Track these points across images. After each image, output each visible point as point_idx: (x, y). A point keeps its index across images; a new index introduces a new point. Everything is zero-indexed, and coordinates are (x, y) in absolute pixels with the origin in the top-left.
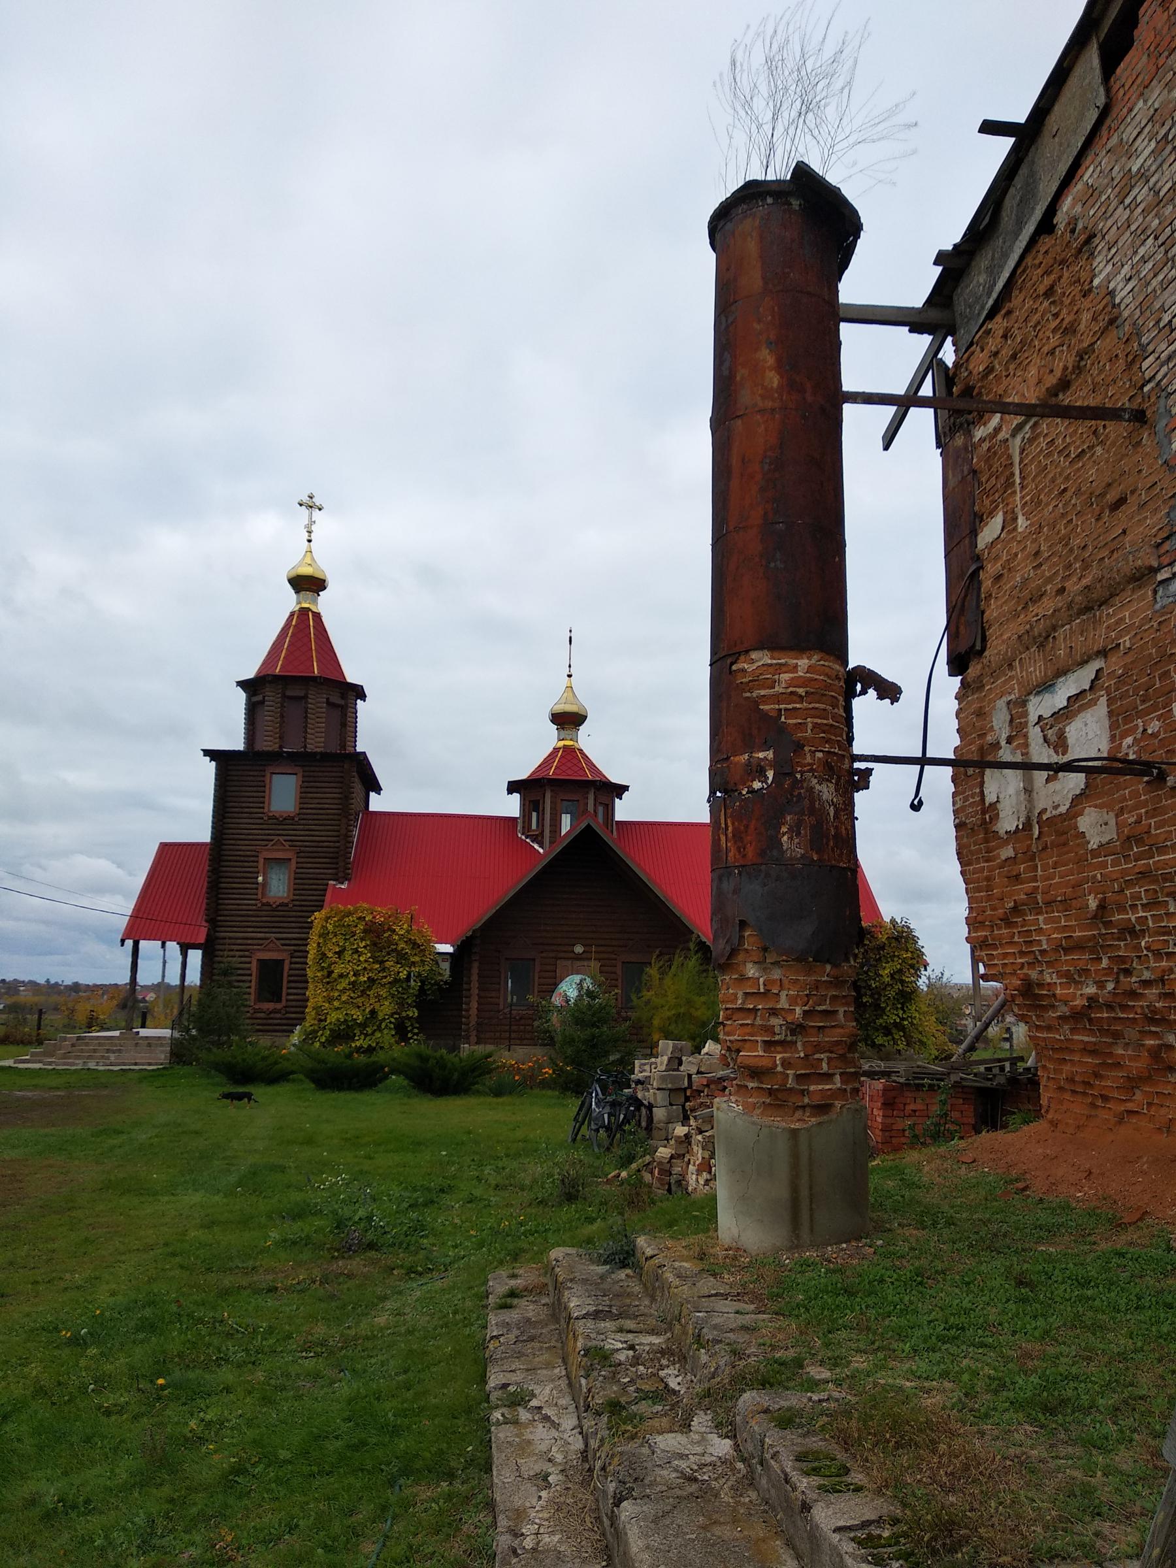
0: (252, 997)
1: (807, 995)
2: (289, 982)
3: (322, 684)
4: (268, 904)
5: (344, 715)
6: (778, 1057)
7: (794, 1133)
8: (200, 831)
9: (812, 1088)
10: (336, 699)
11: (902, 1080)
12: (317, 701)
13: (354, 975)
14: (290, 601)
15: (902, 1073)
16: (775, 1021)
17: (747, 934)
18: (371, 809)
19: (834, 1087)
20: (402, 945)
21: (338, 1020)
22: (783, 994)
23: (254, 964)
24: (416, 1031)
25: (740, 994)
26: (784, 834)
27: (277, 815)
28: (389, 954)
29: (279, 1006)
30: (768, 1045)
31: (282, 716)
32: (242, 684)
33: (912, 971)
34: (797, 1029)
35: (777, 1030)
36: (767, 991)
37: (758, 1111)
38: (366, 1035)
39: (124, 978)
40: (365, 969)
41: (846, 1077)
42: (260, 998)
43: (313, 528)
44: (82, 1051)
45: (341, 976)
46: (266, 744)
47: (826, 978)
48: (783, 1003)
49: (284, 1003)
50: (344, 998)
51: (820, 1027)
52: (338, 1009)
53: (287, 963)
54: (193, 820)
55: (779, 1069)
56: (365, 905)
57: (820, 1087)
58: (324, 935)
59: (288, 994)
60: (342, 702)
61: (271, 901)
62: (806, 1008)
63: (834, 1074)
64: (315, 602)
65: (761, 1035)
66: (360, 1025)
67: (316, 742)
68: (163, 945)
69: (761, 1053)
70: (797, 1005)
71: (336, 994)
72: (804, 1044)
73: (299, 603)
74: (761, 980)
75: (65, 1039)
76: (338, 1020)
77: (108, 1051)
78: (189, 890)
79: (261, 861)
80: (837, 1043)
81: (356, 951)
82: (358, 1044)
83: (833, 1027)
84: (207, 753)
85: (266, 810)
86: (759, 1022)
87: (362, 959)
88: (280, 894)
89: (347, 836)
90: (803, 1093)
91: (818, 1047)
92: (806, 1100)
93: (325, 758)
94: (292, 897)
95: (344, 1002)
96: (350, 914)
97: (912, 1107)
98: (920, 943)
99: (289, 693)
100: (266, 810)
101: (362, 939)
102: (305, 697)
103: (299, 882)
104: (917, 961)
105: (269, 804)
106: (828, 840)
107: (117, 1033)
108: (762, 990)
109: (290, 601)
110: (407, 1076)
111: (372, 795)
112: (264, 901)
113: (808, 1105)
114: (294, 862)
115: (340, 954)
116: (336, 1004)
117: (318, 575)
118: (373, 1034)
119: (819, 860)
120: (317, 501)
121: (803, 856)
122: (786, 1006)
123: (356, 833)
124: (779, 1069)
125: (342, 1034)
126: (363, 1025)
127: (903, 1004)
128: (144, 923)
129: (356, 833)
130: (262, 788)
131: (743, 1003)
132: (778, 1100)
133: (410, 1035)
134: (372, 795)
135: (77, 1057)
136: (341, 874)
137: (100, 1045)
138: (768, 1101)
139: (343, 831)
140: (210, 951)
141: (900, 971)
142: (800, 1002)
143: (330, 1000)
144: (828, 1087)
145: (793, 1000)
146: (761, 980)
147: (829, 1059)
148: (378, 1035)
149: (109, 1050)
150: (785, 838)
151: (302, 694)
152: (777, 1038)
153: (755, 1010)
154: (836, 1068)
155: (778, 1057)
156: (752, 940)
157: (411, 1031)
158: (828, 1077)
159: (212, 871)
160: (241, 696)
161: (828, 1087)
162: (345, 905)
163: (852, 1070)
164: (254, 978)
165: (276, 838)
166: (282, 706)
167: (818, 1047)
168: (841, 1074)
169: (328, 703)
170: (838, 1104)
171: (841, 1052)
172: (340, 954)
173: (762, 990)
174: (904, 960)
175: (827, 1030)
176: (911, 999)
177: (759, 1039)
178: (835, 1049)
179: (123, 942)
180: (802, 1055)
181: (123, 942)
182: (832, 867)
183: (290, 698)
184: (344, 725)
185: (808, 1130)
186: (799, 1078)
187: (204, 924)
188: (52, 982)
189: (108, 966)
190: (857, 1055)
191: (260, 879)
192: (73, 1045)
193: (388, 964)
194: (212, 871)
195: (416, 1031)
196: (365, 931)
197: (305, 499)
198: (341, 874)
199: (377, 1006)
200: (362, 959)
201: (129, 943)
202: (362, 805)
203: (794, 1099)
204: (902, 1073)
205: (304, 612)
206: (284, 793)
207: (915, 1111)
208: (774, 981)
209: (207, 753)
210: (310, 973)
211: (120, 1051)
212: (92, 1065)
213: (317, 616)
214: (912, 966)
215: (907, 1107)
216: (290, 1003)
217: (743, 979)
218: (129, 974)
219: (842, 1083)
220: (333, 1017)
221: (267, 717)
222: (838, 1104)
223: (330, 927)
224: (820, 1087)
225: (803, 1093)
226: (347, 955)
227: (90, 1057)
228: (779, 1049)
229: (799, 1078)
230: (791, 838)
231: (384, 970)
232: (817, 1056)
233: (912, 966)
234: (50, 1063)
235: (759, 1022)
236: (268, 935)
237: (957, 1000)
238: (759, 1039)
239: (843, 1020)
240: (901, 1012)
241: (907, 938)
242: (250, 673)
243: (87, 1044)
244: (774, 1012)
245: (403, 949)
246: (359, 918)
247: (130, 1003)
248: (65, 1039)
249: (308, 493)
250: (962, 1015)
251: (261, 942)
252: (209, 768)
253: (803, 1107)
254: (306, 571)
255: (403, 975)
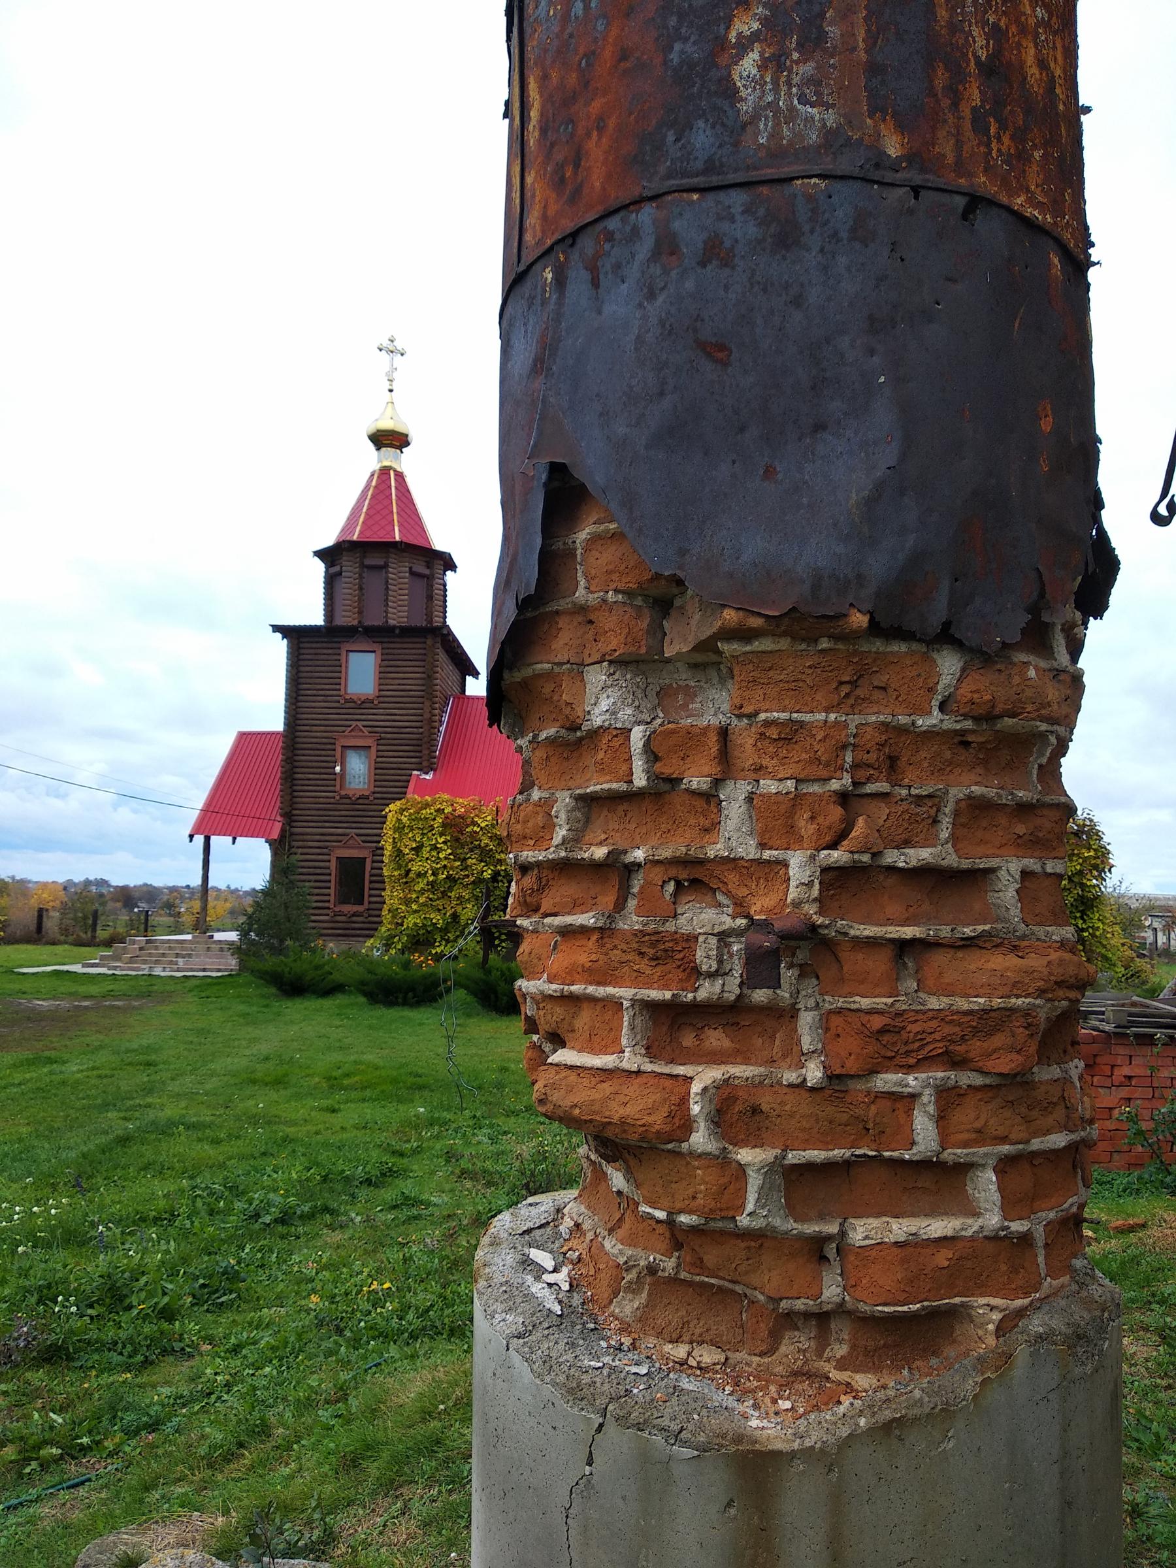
0: (332, 898)
1: (843, 798)
2: (371, 882)
3: (403, 551)
4: (347, 797)
5: (430, 587)
6: (704, 1077)
7: (755, 1471)
8: (274, 720)
9: (862, 1231)
10: (420, 568)
11: (1108, 1028)
12: (399, 571)
13: (433, 874)
14: (371, 460)
15: (1109, 1015)
16: (702, 918)
17: (582, 536)
18: (468, 693)
19: (972, 1226)
20: (486, 841)
21: (415, 924)
22: (735, 796)
23: (334, 861)
24: (504, 937)
25: (564, 801)
26: (744, 45)
27: (355, 698)
28: (471, 850)
29: (360, 908)
30: (670, 1024)
31: (361, 589)
32: (321, 554)
33: (1095, 873)
34: (793, 948)
35: (705, 956)
36: (664, 786)
37: (627, 1306)
38: (448, 941)
39: (196, 881)
40: (445, 867)
41: (1025, 1176)
42: (343, 899)
43: (395, 375)
44: (150, 955)
45: (419, 875)
46: (345, 619)
47: (933, 719)
48: (734, 834)
49: (366, 905)
50: (422, 900)
51: (903, 947)
52: (416, 912)
53: (368, 862)
54: (261, 700)
55: (701, 1139)
56: (445, 796)
57: (900, 1228)
58: (399, 828)
59: (370, 896)
60: (427, 572)
61: (350, 794)
62: (836, 856)
63: (964, 1169)
64: (397, 459)
65: (638, 980)
66: (441, 930)
67: (398, 617)
68: (234, 839)
69: (630, 1060)
70: (792, 839)
71: (414, 896)
72: (826, 1020)
73: (380, 461)
74: (637, 736)
75: (134, 942)
76: (415, 924)
77: (177, 955)
78: (276, 783)
79: (339, 749)
80: (987, 1022)
81: (434, 848)
82: (439, 950)
83: (969, 944)
84: (276, 628)
85: (342, 692)
86: (632, 921)
87: (441, 856)
88: (361, 786)
89: (431, 721)
90: (817, 1250)
91: (893, 1042)
92: (831, 1291)
93: (407, 632)
94: (372, 789)
95: (423, 905)
96: (427, 805)
97: (1126, 1071)
98: (1106, 839)
99: (367, 562)
100: (342, 692)
101: (441, 835)
102: (386, 566)
103: (379, 771)
104: (1100, 862)
105: (346, 686)
106: (958, 76)
107: (189, 937)
108: (640, 780)
109: (371, 460)
110: (466, 988)
111: (469, 679)
112: (343, 793)
113: (841, 1310)
114: (374, 750)
115: (417, 850)
116: (414, 907)
117: (400, 429)
118: (455, 940)
119: (912, 158)
120: (399, 345)
121: (832, 139)
122: (748, 849)
123: (445, 719)
124: (701, 1139)
125: (420, 941)
126: (445, 930)
127: (1083, 913)
128: (220, 817)
129: (445, 719)
130: (338, 670)
131: (575, 839)
132: (707, 1277)
133: (497, 942)
134: (469, 679)
135: (145, 962)
136: (425, 764)
137: (170, 948)
138: (669, 1265)
139: (427, 716)
140: (279, 848)
141: (1080, 873)
142: (806, 828)
143: (407, 902)
144: (937, 1227)
145: (777, 823)
146: (637, 736)
147: (948, 1097)
148: (461, 941)
149: (180, 956)
150: (749, 64)
151: (381, 562)
152: (706, 991)
153: (617, 870)
154: (981, 1136)
155: (704, 1077)
156: (606, 557)
157: (498, 938)
158: (940, 1180)
159: (285, 761)
160: (319, 567)
161: (937, 1227)
162: (422, 796)
163: (1059, 1140)
164: (333, 878)
165: (354, 724)
166: (361, 577)
167: (893, 1042)
168: (1004, 1166)
169: (412, 573)
170: (988, 1308)
171: (1006, 1064)
172: (417, 850)
173: (640, 780)
174: (1085, 859)
175: (940, 959)
176: (1092, 906)
177: (625, 993)
178: (976, 1047)
179: (191, 837)
180: (814, 1073)
181: (191, 837)
182: (976, 202)
183: (370, 567)
184: (430, 598)
185: (826, 1459)
186: (796, 1182)
187: (279, 818)
188: (233, 888)
189: (172, 866)
190: (1076, 1067)
191: (338, 769)
192: (141, 949)
193: (470, 862)
194: (285, 761)
195: (504, 937)
196: (444, 825)
197: (386, 343)
198: (425, 764)
199: (459, 909)
200: (441, 856)
201: (199, 839)
202: (457, 690)
203: (769, 1280)
204: (1109, 1015)
205: (385, 471)
206: (362, 672)
207: (1130, 1078)
208: (694, 737)
209: (276, 628)
210: (386, 872)
211: (190, 956)
212: (158, 971)
213: (400, 476)
214: (1096, 867)
215: (1116, 1071)
216: (373, 906)
217: (578, 741)
218: (201, 872)
219: (1011, 1205)
220: (411, 921)
221: (345, 589)
222: (988, 1308)
223: (404, 820)
224: (900, 1228)
225: (817, 1250)
226: (425, 853)
227: (157, 962)
228: (716, 1039)
229: (796, 1182)
230: (775, 63)
231: (466, 869)
232: (887, 1081)
233: (1096, 867)
234: (115, 968)
235: (632, 921)
236: (348, 831)
237: (1137, 910)
238: (625, 993)
239: (1015, 913)
240: (1080, 922)
241: (1088, 833)
242: (329, 541)
243: (156, 948)
244: (695, 877)
245: (487, 845)
246: (438, 810)
247: (197, 906)
248: (134, 942)
249: (389, 336)
250: (1141, 927)
251: (340, 838)
252: (280, 646)
253: (822, 1319)
254: (386, 424)
255: (487, 875)
